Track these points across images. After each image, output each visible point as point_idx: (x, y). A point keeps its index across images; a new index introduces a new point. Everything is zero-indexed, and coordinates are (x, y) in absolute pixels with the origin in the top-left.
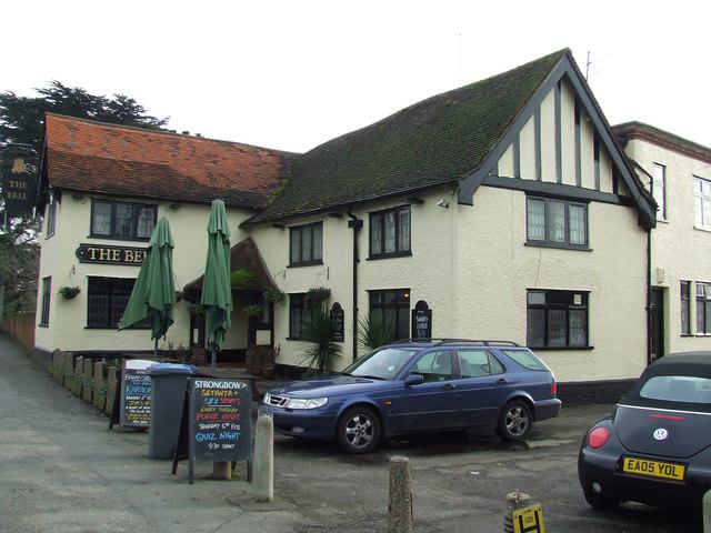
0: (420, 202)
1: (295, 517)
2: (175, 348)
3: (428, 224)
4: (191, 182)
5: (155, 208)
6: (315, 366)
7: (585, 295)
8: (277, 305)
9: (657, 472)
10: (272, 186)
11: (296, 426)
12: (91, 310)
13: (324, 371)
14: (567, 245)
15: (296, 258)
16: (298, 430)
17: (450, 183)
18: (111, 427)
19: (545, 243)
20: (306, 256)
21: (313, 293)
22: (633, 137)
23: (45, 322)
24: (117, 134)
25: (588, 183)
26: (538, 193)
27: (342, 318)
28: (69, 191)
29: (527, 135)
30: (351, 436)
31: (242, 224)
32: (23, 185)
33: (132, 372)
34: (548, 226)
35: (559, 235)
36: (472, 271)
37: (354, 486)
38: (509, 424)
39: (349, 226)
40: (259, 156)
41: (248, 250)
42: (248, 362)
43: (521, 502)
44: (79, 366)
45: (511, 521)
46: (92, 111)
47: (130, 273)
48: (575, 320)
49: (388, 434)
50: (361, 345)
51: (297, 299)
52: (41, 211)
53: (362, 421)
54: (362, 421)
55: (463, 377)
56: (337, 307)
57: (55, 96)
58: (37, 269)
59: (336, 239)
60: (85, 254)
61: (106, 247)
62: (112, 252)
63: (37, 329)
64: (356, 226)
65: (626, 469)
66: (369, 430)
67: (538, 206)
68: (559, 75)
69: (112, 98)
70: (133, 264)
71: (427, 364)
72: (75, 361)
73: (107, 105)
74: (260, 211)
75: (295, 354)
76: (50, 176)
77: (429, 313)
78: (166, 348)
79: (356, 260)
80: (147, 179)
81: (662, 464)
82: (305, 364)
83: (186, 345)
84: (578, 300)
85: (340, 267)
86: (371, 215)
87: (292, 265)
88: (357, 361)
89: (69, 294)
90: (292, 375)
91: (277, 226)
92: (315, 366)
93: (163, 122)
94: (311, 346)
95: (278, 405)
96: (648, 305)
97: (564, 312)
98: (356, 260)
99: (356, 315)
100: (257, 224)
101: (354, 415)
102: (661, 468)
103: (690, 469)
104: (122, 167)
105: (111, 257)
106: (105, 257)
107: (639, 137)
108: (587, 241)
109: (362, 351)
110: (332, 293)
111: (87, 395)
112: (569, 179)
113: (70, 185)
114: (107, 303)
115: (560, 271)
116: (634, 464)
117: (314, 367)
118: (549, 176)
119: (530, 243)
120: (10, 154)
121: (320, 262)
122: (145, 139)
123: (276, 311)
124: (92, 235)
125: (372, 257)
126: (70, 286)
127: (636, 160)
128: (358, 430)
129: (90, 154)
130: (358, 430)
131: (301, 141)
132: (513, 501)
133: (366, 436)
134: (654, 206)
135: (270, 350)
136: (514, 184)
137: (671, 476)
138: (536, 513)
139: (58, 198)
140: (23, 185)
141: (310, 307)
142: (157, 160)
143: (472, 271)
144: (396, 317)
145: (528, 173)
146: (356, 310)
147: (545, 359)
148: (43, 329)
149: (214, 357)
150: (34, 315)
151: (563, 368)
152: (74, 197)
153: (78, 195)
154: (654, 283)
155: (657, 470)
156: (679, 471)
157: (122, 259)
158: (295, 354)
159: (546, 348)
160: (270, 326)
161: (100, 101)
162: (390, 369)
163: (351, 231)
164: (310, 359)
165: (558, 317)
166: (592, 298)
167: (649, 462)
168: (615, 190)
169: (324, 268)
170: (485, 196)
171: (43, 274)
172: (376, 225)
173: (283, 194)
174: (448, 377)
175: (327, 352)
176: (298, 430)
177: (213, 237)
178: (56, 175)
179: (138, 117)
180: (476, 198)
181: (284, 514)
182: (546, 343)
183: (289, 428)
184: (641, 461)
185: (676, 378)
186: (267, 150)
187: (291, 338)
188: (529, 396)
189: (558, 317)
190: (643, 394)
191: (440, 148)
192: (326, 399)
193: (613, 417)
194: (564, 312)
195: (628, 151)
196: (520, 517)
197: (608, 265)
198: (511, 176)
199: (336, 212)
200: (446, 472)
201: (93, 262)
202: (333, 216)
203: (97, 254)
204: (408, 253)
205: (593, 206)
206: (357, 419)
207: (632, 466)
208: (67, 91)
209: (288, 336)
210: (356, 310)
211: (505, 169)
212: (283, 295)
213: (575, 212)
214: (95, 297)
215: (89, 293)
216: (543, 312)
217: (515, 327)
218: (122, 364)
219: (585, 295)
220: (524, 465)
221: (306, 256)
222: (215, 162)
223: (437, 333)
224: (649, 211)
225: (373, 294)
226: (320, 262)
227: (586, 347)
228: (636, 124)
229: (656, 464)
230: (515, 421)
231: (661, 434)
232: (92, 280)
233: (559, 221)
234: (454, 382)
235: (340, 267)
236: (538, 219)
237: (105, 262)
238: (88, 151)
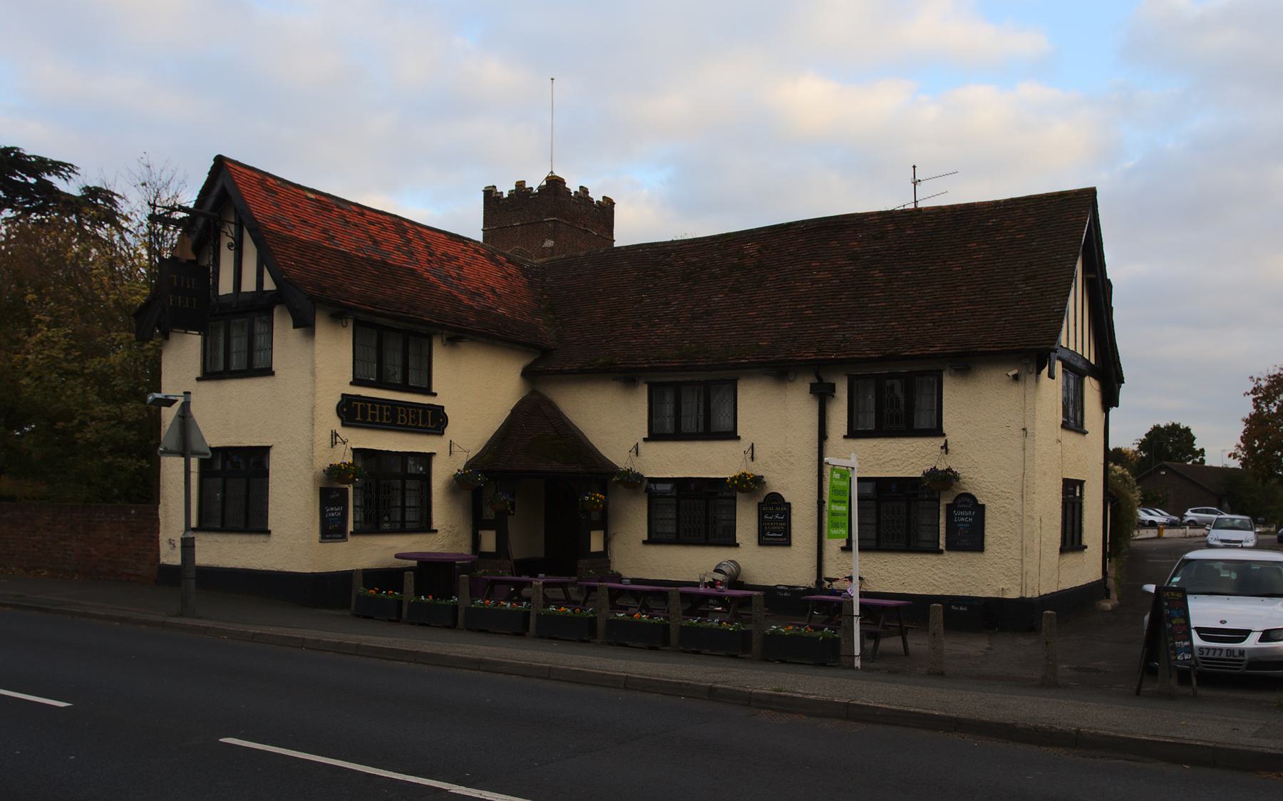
5: (428, 338)
50: (833, 546)
64: (823, 395)
79: (823, 436)
98: (823, 436)
105: (381, 418)
106: (374, 416)
120: (2, 243)
124: (356, 382)
169: (743, 445)
182: (223, 523)
203: (364, 410)
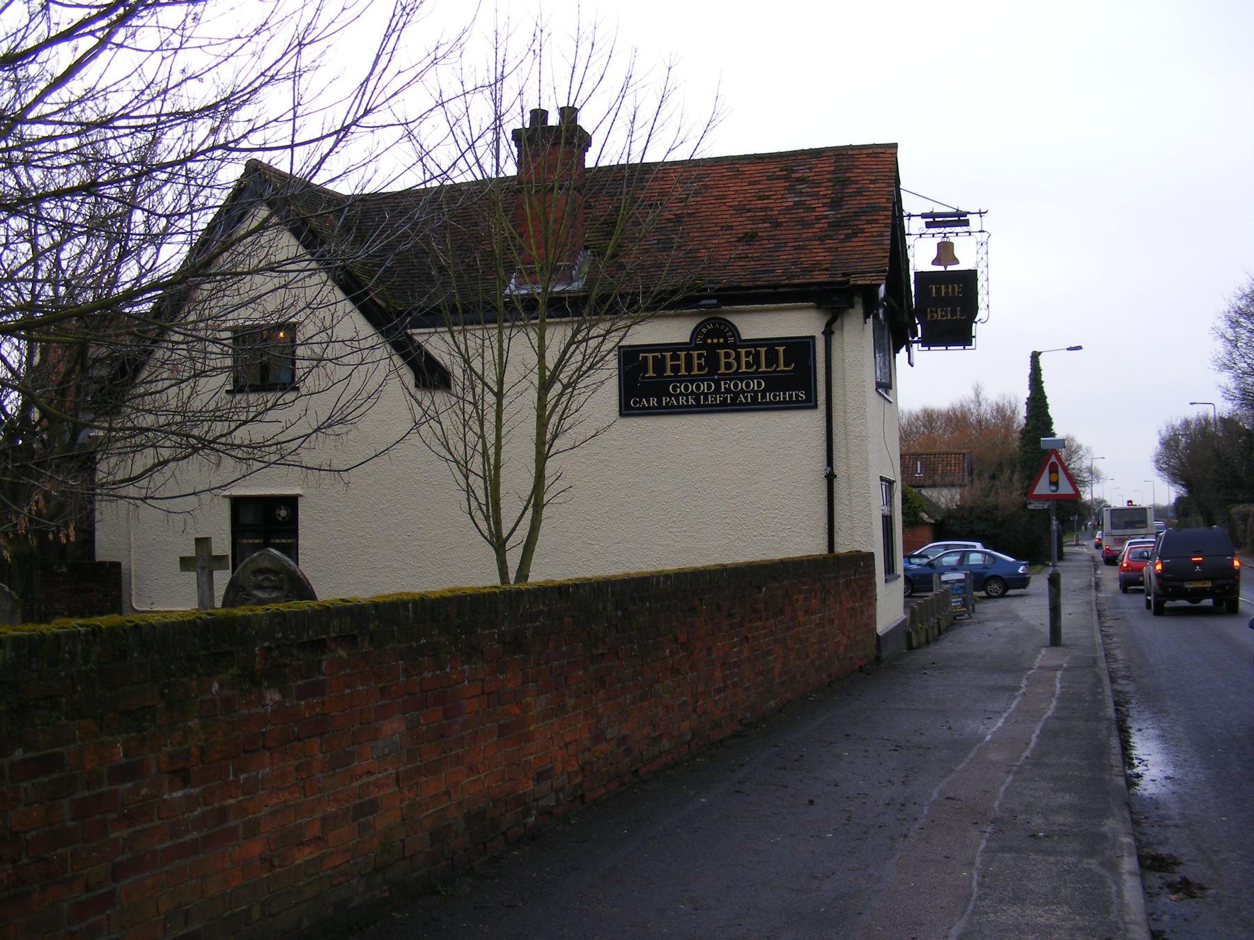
105: (689, 367)
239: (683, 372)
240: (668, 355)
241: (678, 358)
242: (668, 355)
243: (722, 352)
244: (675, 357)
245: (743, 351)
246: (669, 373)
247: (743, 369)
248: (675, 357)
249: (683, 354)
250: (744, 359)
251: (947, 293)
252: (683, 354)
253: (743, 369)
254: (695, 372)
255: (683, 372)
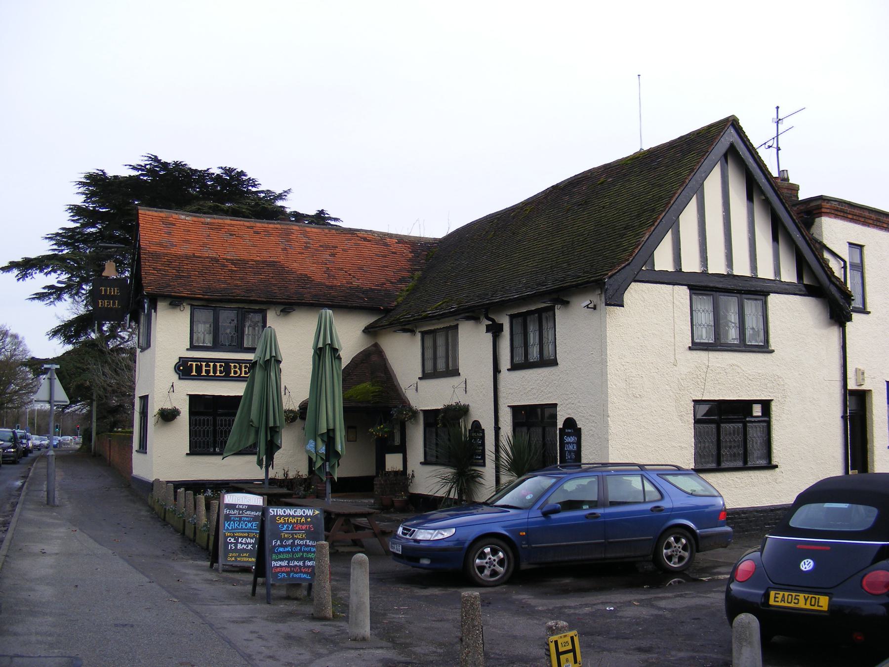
0: (566, 303)
1: (390, 654)
2: (291, 475)
3: (571, 326)
4: (305, 280)
6: (454, 495)
7: (766, 405)
8: (408, 425)
9: (802, 605)
10: (402, 280)
11: (424, 557)
12: (193, 434)
13: (464, 501)
14: (743, 347)
15: (429, 368)
16: (425, 562)
17: (596, 281)
18: (212, 566)
19: (717, 345)
20: (441, 366)
21: (448, 409)
22: (820, 214)
23: (143, 448)
24: (219, 228)
25: (766, 271)
26: (701, 286)
27: (483, 438)
28: (164, 297)
29: (688, 219)
30: (482, 569)
31: (366, 328)
32: (115, 291)
33: (232, 507)
34: (718, 326)
35: (733, 335)
36: (635, 379)
37: (433, 616)
38: (480, 558)
39: (487, 331)
40: (386, 245)
41: (374, 358)
42: (377, 490)
43: (557, 628)
44: (181, 500)
45: (548, 645)
46: (194, 188)
47: (236, 389)
48: (755, 433)
49: (524, 566)
51: (431, 416)
52: (135, 318)
53: (494, 552)
54: (494, 552)
55: (613, 504)
56: (477, 425)
57: (151, 172)
58: (132, 388)
59: (473, 345)
60: (184, 369)
61: (208, 361)
62: (215, 366)
63: (135, 455)
64: (495, 330)
65: (772, 602)
66: (501, 562)
67: (705, 305)
68: (720, 145)
69: (217, 171)
70: (239, 379)
71: (574, 486)
72: (175, 492)
73: (212, 179)
74: (387, 311)
75: (430, 481)
76: (144, 282)
77: (578, 432)
78: (280, 476)
79: (496, 370)
80: (252, 279)
81: (806, 596)
82: (441, 493)
83: (304, 472)
84: (757, 411)
85: (477, 378)
86: (512, 317)
87: (425, 376)
88: (501, 490)
89: (168, 416)
90: (425, 507)
91: (405, 331)
92: (454, 495)
93: (280, 197)
94: (448, 472)
95: (408, 537)
96: (845, 411)
97: (740, 425)
98: (496, 370)
99: (499, 434)
100: (384, 327)
101: (486, 546)
102: (806, 600)
103: (834, 599)
104: (224, 266)
105: (215, 372)
106: (208, 372)
107: (828, 214)
108: (767, 341)
109: (505, 479)
110: (471, 409)
111: (189, 532)
112: (742, 268)
113: (166, 291)
114: (211, 424)
115: (733, 377)
116: (780, 596)
117: (451, 496)
118: (717, 266)
119: (696, 346)
121: (455, 373)
122: (252, 231)
123: (408, 432)
124: (193, 347)
125: (514, 367)
126: (168, 406)
127: (825, 242)
128: (490, 560)
129: (190, 253)
130: (490, 560)
131: (437, 229)
132: (550, 628)
133: (487, 572)
134: (848, 297)
135: (403, 477)
136: (675, 278)
137: (816, 608)
138: (572, 638)
139: (154, 306)
140: (115, 291)
141: (444, 425)
142: (265, 256)
143: (635, 379)
144: (546, 439)
145: (691, 264)
146: (497, 429)
147: (715, 479)
148: (141, 456)
149: (329, 488)
150: (131, 439)
151: (739, 491)
152: (170, 304)
153: (175, 302)
154: (851, 385)
155: (802, 602)
156: (824, 602)
157: (226, 373)
158: (430, 481)
159: (719, 469)
160: (402, 449)
161: (203, 175)
162: (528, 497)
163: (490, 335)
164: (447, 488)
165: (733, 431)
166: (774, 407)
167: (794, 594)
168: (800, 276)
170: (637, 294)
171: (139, 393)
172: (518, 329)
173: (414, 290)
174: (593, 504)
175: (466, 479)
176: (425, 562)
177: (319, 353)
178: (150, 279)
179: (249, 192)
180: (628, 297)
181: (380, 651)
182: (719, 463)
183: (417, 560)
184: (786, 594)
185: (827, 505)
186: (396, 236)
187: (426, 463)
188: (692, 525)
189: (733, 431)
190: (794, 522)
191: (583, 237)
192: (454, 530)
193: (762, 551)
194: (740, 425)
195: (814, 230)
196: (556, 642)
197: (797, 370)
198: (671, 269)
199: (473, 314)
200: (572, 611)
201: (193, 378)
202: (468, 318)
203: (199, 369)
204: (554, 363)
205: (772, 299)
206: (487, 550)
207: (778, 599)
208: (166, 165)
209: (422, 460)
210: (497, 429)
211: (663, 260)
212: (414, 413)
213: (751, 308)
214: (198, 418)
215: (191, 413)
216: (714, 426)
217: (678, 445)
218: (219, 498)
219: (766, 405)
220: (662, 604)
221: (441, 366)
222: (333, 255)
223: (588, 456)
224: (842, 302)
225: (516, 410)
226: (455, 373)
227: (773, 467)
228: (821, 198)
229: (802, 595)
230: (674, 552)
231: (807, 565)
232: (194, 400)
233: (733, 317)
234: (599, 511)
235: (477, 378)
236: (705, 317)
237: (208, 378)
238: (184, 249)
239: (212, 374)
240: (204, 364)
241: (209, 366)
242: (204, 364)
243: (232, 365)
244: (208, 366)
245: (218, 364)
246: (204, 374)
247: (243, 375)
248: (208, 366)
249: (212, 364)
250: (243, 369)
251: (110, 292)
252: (212, 364)
253: (243, 375)
254: (218, 374)
255: (212, 374)
